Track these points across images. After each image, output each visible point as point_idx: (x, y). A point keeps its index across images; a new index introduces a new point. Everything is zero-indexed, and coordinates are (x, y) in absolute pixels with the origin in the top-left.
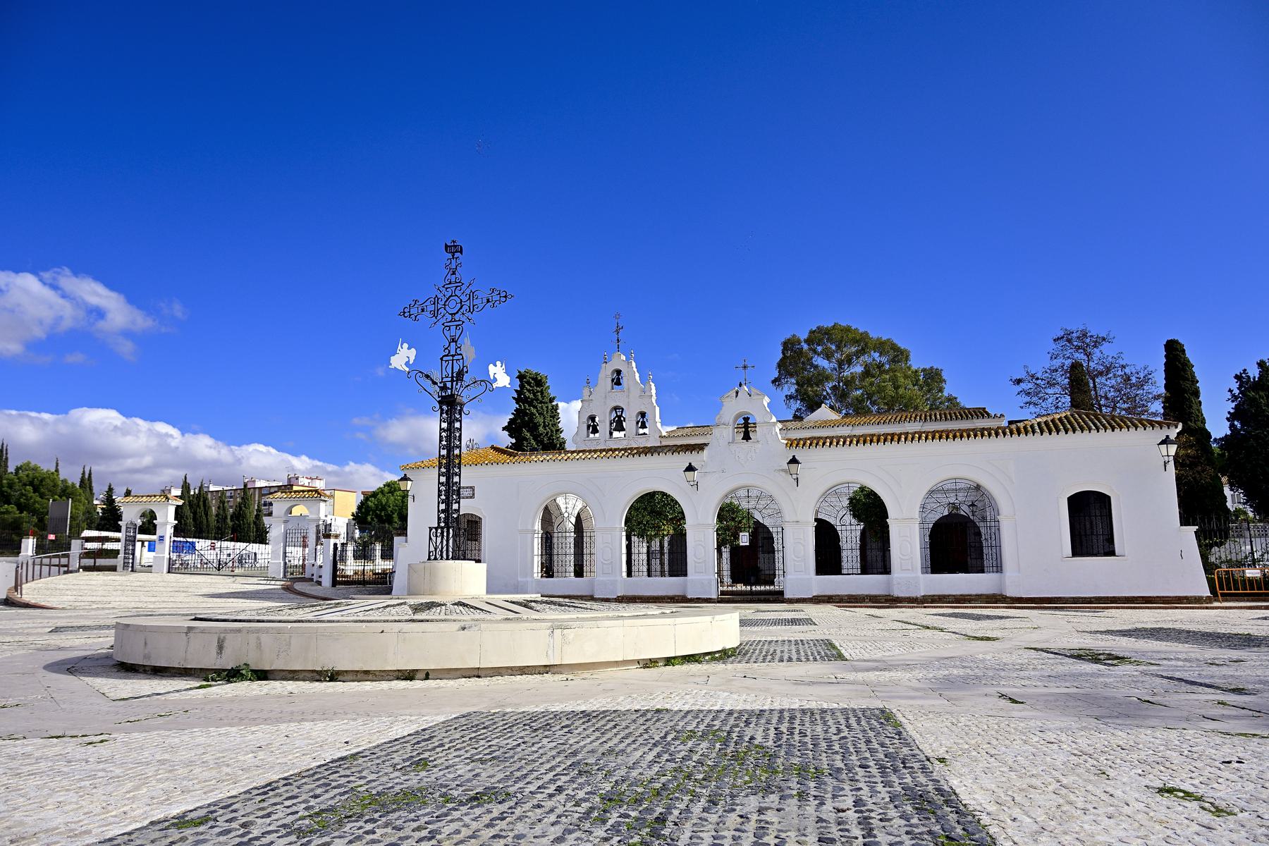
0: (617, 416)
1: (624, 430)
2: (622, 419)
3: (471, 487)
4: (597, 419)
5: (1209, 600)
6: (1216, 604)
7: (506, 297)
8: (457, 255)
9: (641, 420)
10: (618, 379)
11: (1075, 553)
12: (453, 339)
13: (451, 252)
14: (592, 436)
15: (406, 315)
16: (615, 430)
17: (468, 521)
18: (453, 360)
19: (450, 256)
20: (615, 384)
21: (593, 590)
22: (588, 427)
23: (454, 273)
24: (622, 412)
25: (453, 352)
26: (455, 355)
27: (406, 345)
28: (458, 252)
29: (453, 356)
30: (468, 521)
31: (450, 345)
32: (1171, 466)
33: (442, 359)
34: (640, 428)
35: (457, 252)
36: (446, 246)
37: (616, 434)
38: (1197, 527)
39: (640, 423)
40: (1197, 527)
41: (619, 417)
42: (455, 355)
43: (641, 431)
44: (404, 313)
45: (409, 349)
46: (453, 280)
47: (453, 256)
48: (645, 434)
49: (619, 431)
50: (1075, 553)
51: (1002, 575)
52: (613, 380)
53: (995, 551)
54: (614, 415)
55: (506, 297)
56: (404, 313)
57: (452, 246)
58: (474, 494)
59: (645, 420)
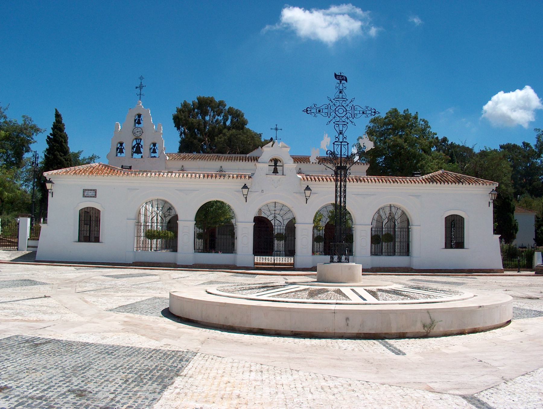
0: (137, 143)
1: (141, 153)
2: (140, 146)
3: (94, 190)
4: (124, 145)
5: (502, 271)
6: (506, 273)
7: (375, 112)
8: (343, 82)
9: (153, 148)
10: (139, 120)
11: (446, 247)
12: (341, 132)
13: (339, 79)
14: (119, 154)
15: (308, 112)
16: (135, 152)
17: (85, 211)
18: (341, 145)
19: (339, 81)
20: (137, 123)
21: (38, 245)
22: (117, 149)
23: (341, 92)
24: (140, 141)
25: (341, 140)
26: (342, 142)
27: (327, 135)
28: (344, 80)
29: (341, 142)
30: (85, 211)
31: (339, 135)
32: (492, 205)
33: (334, 143)
34: (152, 153)
35: (343, 80)
36: (335, 74)
37: (135, 155)
38: (500, 235)
39: (152, 150)
40: (500, 235)
41: (138, 144)
42: (342, 142)
43: (153, 155)
44: (307, 111)
45: (328, 137)
46: (341, 96)
47: (341, 82)
48: (155, 157)
49: (138, 154)
50: (446, 247)
51: (411, 257)
52: (135, 120)
53: (402, 244)
54: (135, 143)
55: (375, 112)
56: (307, 111)
57: (339, 76)
58: (96, 195)
59: (155, 148)
